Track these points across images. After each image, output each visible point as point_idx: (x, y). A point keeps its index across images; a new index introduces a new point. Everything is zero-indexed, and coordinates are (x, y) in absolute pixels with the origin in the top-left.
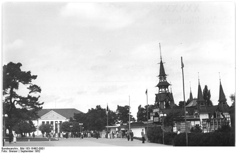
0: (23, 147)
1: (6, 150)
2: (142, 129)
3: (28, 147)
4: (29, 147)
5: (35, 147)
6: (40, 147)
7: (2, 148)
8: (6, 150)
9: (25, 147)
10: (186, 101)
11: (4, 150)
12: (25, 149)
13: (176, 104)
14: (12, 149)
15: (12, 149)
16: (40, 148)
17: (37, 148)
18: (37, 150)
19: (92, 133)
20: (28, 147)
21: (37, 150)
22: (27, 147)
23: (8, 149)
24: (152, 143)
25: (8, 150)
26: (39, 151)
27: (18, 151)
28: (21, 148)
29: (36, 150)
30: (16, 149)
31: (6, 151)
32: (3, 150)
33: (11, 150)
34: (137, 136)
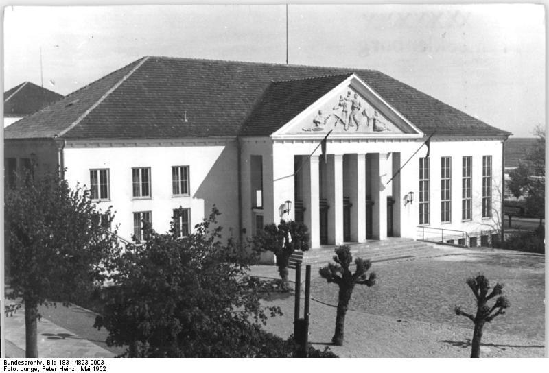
0: (54, 359)
1: (13, 366)
2: (289, 63)
3: (66, 359)
4: (68, 359)
5: (78, 359)
6: (94, 359)
7: (5, 362)
8: (13, 366)
9: (58, 360)
10: (319, 143)
11: (10, 366)
12: (58, 363)
13: (293, 143)
14: (27, 363)
15: (27, 363)
16: (94, 362)
17: (82, 362)
18: (99, 366)
19: (114, 302)
20: (66, 359)
21: (99, 366)
22: (62, 359)
23: (19, 363)
24: (546, 287)
25: (20, 367)
26: (103, 369)
27: (76, 369)
28: (48, 362)
29: (95, 366)
30: (37, 363)
31: (88, 369)
32: (7, 365)
33: (25, 366)
34: (291, 269)
